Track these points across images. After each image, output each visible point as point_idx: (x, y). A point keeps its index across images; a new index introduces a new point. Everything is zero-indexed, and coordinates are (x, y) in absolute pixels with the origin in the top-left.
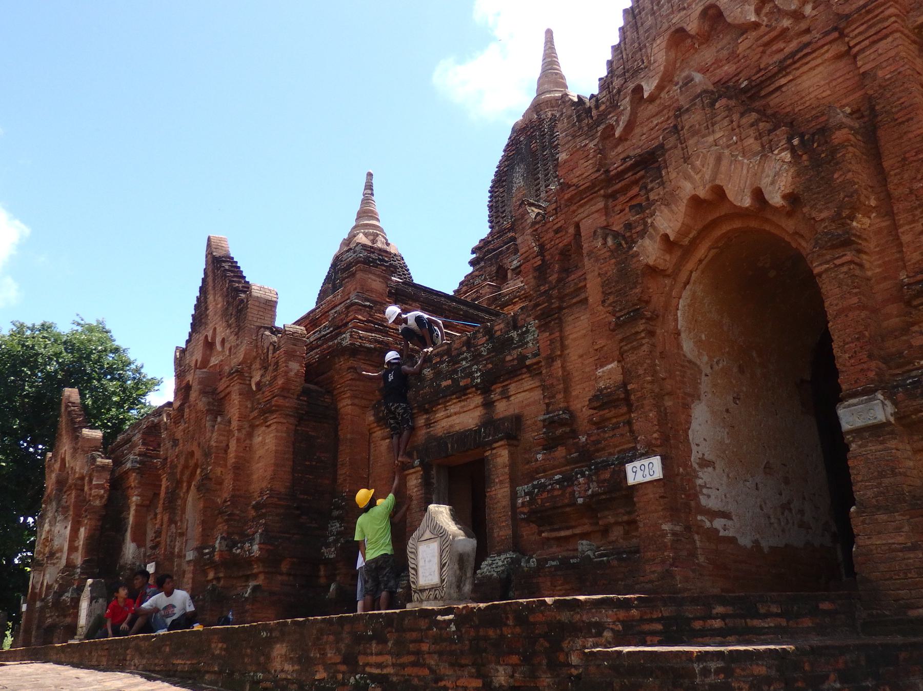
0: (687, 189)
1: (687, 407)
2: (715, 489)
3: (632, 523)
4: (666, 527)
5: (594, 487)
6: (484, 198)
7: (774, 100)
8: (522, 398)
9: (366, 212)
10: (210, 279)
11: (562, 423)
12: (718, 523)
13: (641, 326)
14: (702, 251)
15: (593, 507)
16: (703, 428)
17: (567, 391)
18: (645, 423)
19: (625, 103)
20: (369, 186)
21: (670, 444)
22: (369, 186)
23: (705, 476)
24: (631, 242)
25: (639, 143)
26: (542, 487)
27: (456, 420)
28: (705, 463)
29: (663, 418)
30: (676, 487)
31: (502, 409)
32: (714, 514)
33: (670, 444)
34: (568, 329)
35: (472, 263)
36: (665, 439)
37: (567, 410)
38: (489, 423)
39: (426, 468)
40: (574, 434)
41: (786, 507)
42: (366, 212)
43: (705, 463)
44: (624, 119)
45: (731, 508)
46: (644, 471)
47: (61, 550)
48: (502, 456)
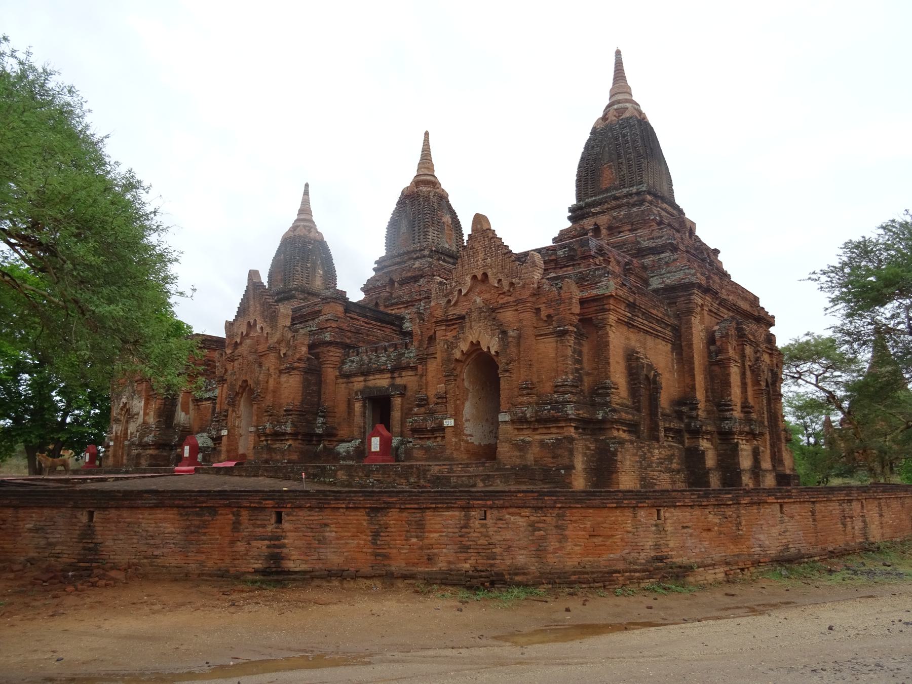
0: (471, 338)
1: (463, 403)
2: (469, 428)
3: (444, 437)
4: (454, 440)
5: (433, 425)
6: (383, 232)
7: (499, 315)
8: (407, 379)
9: (305, 210)
10: (251, 293)
11: (424, 400)
12: (469, 438)
13: (452, 378)
14: (473, 356)
15: (433, 430)
16: (468, 409)
17: (426, 389)
18: (451, 408)
19: (456, 293)
20: (306, 193)
21: (457, 415)
22: (306, 193)
23: (467, 424)
24: (452, 349)
25: (460, 310)
26: (416, 421)
27: (378, 381)
28: (467, 420)
29: (456, 407)
30: (458, 429)
31: (399, 381)
32: (467, 435)
33: (457, 415)
34: (429, 366)
35: (374, 269)
36: (456, 415)
37: (426, 395)
38: (392, 385)
39: (364, 399)
40: (428, 404)
41: (491, 432)
42: (305, 210)
43: (467, 420)
44: (455, 299)
45: (473, 433)
46: (449, 422)
47: (138, 414)
48: (397, 401)
